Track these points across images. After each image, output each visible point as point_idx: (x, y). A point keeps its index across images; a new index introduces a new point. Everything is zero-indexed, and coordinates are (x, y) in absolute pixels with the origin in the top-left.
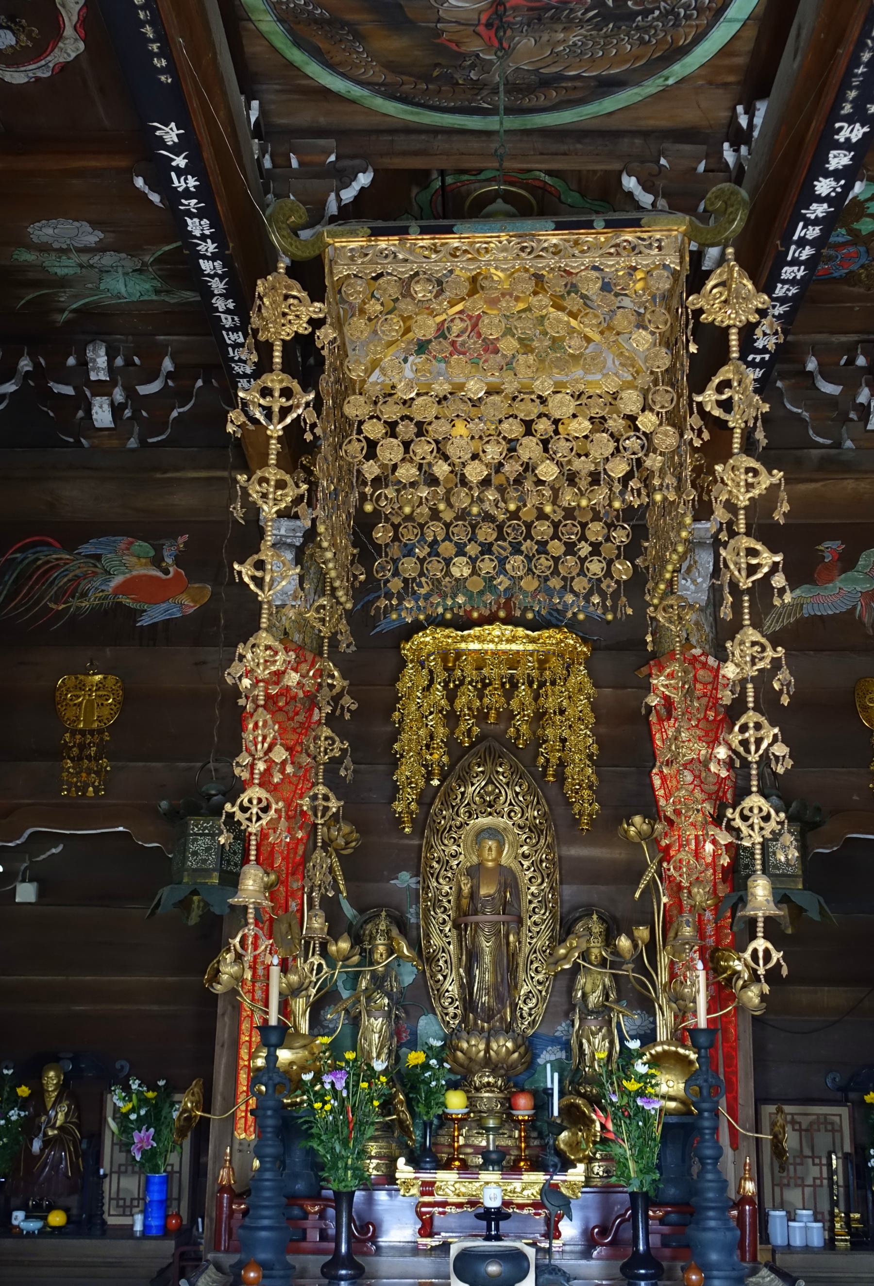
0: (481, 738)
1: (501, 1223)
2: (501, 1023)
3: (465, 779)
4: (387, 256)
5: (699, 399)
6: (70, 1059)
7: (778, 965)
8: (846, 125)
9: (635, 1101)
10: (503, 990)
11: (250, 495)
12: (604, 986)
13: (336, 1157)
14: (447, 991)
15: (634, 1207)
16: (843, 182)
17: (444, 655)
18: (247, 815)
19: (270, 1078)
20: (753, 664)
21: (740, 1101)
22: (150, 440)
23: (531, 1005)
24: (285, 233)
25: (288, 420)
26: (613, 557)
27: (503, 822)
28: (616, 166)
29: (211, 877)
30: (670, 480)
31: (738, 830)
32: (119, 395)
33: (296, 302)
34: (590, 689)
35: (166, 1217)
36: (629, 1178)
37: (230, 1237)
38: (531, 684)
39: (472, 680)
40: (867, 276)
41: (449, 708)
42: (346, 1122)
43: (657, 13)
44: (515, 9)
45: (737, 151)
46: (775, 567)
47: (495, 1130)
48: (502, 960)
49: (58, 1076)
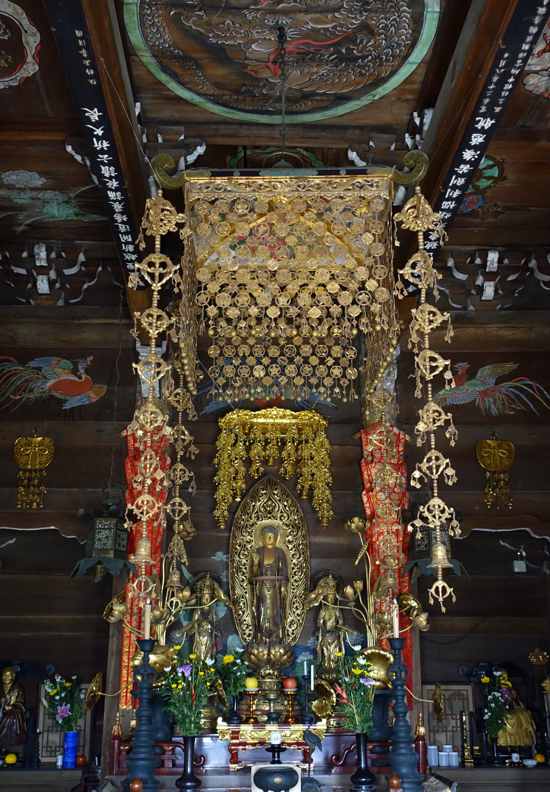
0: (264, 474)
1: (281, 753)
2: (277, 638)
3: (255, 498)
4: (220, 189)
5: (401, 272)
6: (19, 664)
7: (450, 596)
8: (482, 119)
9: (359, 681)
10: (278, 619)
11: (142, 324)
12: (336, 616)
13: (185, 716)
14: (245, 620)
15: (358, 742)
16: (479, 152)
17: (244, 425)
18: (141, 511)
19: (145, 671)
20: (434, 423)
21: (413, 682)
22: (71, 301)
23: (293, 628)
24: (162, 173)
25: (164, 281)
26: (347, 366)
27: (277, 522)
28: (345, 146)
29: (109, 554)
30: (385, 318)
31: (427, 518)
32: (53, 275)
33: (168, 213)
34: (327, 445)
35: (77, 757)
36: (355, 725)
37: (119, 766)
38: (293, 442)
39: (260, 440)
40: (482, 213)
41: (247, 456)
42: (191, 696)
43: (370, 57)
44: (290, 53)
45: (413, 138)
46: (446, 368)
47: (274, 700)
48: (277, 602)
49: (12, 675)
